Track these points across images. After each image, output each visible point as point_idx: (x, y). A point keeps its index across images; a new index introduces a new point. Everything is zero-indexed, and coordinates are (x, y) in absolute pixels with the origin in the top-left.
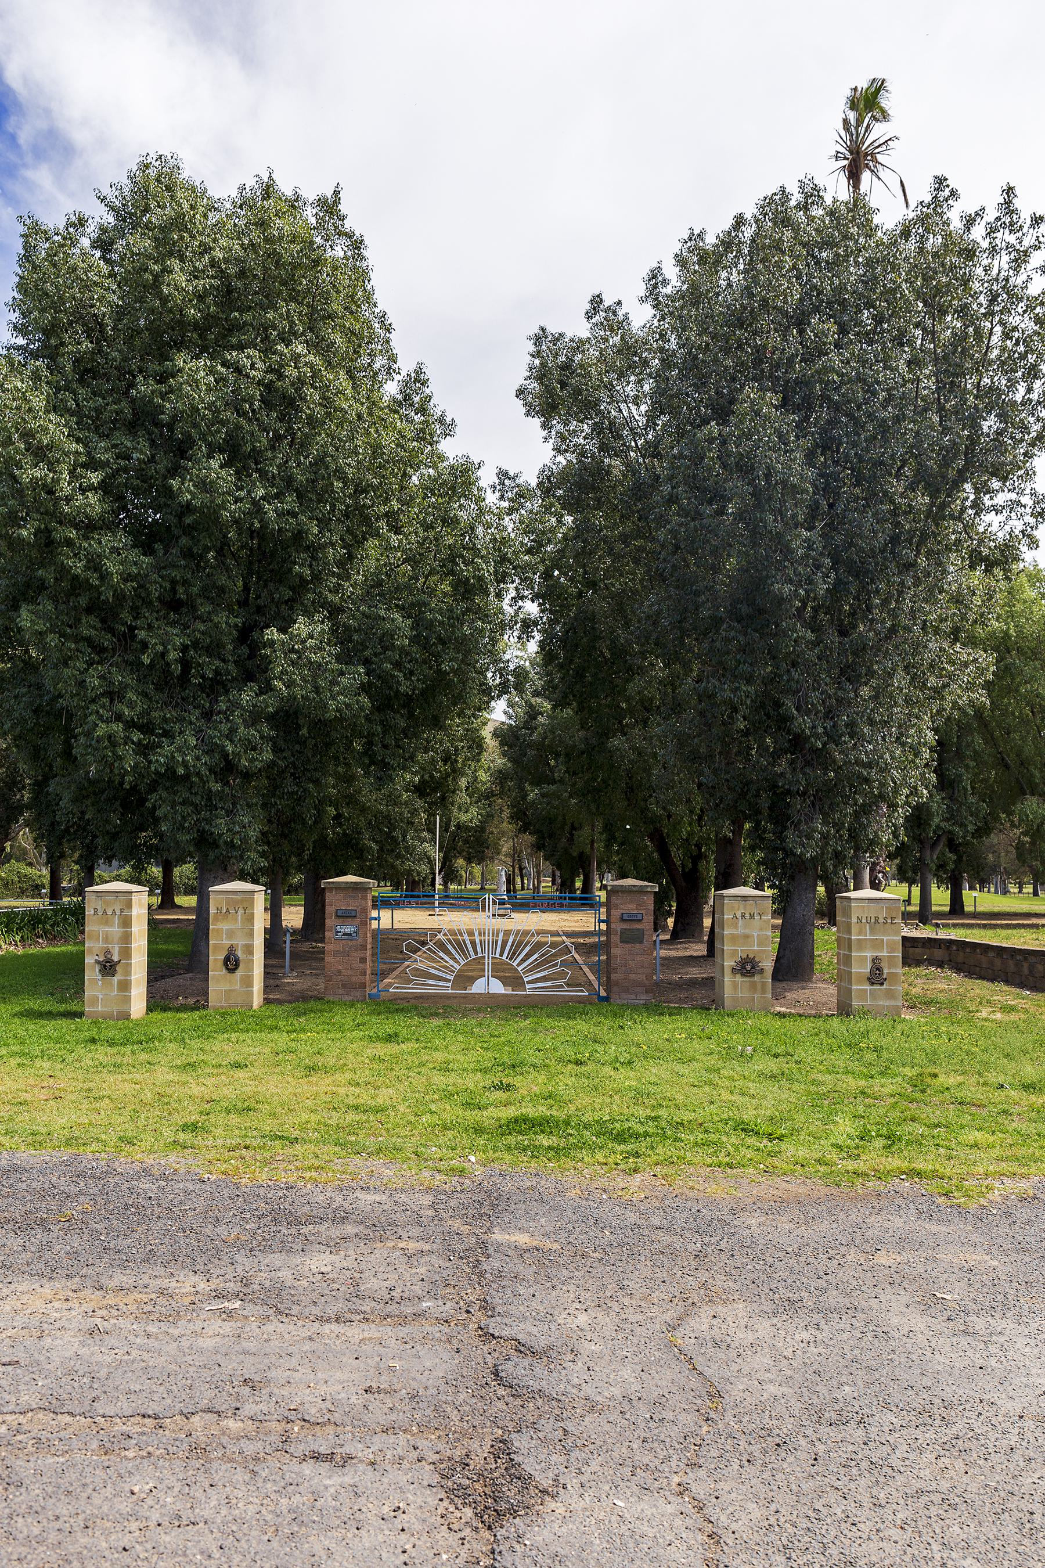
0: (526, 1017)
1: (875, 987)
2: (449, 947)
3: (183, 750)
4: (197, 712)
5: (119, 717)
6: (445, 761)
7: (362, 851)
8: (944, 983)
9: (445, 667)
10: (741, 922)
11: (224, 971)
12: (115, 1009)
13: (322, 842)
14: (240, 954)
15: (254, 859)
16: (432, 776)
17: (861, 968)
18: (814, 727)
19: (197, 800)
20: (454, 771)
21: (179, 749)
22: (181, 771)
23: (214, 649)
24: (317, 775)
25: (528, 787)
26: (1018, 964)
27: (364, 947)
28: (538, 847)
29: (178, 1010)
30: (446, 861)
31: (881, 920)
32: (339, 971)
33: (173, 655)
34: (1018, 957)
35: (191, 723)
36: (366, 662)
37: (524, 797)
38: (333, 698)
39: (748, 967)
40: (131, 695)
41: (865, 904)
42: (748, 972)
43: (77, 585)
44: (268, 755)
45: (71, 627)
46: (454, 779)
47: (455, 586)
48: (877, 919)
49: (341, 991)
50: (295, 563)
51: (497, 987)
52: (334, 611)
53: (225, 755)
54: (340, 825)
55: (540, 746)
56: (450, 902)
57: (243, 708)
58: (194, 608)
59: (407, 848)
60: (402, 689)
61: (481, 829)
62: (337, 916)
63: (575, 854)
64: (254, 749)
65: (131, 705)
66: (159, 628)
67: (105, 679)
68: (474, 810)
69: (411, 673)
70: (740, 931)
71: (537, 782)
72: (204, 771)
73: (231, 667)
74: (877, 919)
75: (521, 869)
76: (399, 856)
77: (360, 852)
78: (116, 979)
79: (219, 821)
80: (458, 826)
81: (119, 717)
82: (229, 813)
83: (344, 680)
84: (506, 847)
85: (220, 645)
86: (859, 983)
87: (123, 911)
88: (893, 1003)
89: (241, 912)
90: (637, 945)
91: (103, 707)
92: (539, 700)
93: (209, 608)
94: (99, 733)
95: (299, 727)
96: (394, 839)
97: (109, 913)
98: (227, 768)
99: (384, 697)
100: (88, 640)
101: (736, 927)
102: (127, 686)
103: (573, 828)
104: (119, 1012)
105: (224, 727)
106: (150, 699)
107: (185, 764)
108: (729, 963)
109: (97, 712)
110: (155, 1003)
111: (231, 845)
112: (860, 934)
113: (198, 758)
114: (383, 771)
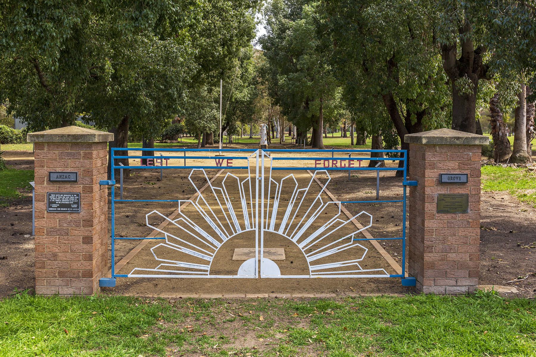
2: (208, 219)
6: (223, 45)
24: (58, 13)
25: (279, 77)
27: (89, 223)
28: (284, 113)
32: (55, 255)
37: (276, 84)
46: (230, 59)
49: (58, 281)
55: (287, 50)
61: (250, 102)
62: (50, 181)
63: (309, 116)
68: (246, 91)
71: (286, 72)
75: (272, 127)
84: (265, 115)
90: (459, 216)
92: (287, 20)
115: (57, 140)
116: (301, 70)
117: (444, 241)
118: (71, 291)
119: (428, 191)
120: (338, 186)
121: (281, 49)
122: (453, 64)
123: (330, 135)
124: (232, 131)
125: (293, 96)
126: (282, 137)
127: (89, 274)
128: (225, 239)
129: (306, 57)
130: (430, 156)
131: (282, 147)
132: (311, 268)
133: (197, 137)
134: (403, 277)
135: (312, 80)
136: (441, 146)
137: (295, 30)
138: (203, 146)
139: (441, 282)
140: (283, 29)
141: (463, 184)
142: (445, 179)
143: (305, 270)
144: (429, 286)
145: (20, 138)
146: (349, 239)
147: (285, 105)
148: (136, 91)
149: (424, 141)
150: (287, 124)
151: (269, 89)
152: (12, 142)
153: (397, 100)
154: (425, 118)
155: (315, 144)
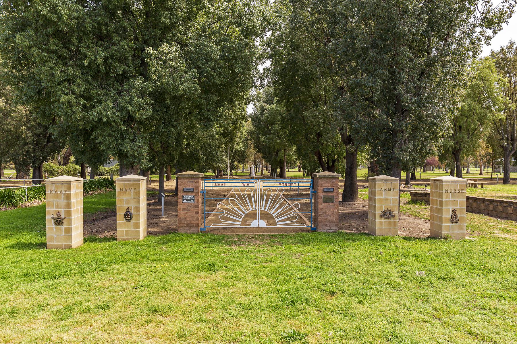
0: (281, 243)
1: (453, 224)
3: (107, 109)
4: (114, 91)
5: (73, 92)
6: (233, 124)
7: (198, 159)
8: (479, 219)
9: (237, 71)
10: (384, 193)
11: (125, 221)
12: (63, 243)
13: (181, 155)
14: (132, 211)
15: (146, 163)
16: (228, 130)
17: (447, 215)
18: (411, 99)
19: (115, 134)
20: (236, 128)
21: (104, 109)
22: (105, 120)
23: (123, 60)
26: (487, 206)
27: (197, 206)
29: (101, 241)
30: (232, 163)
31: (457, 191)
32: (185, 218)
33: (99, 61)
34: (486, 203)
35: (111, 96)
36: (199, 68)
37: (259, 140)
38: (181, 84)
39: (388, 214)
40: (79, 81)
41: (449, 183)
42: (388, 216)
43: (48, 22)
44: (150, 112)
45: (45, 45)
46: (236, 131)
47: (242, 31)
48: (455, 191)
49: (186, 228)
50: (162, 16)
51: (263, 224)
52: (183, 45)
53: (128, 112)
54: (189, 148)
55: (266, 121)
56: (233, 178)
57: (136, 88)
58: (111, 39)
59: (218, 158)
60: (216, 81)
63: (278, 160)
64: (143, 109)
65: (79, 86)
66: (92, 47)
67: (65, 73)
68: (241, 144)
69: (220, 74)
70: (384, 197)
71: (264, 134)
72: (118, 120)
73: (132, 69)
74: (455, 191)
76: (215, 161)
77: (198, 160)
78: (63, 227)
79: (126, 145)
80: (236, 151)
81: (73, 92)
82: (132, 141)
83: (187, 76)
85: (126, 59)
86: (446, 222)
87: (67, 191)
88: (461, 231)
89: (133, 190)
90: (331, 204)
91: (65, 87)
92: (265, 104)
93: (119, 38)
94: (62, 100)
95: (165, 99)
96: (213, 154)
97: (59, 192)
98: (129, 119)
99: (208, 88)
100: (55, 52)
101: (382, 195)
102: (77, 76)
103: (278, 151)
104: (65, 245)
105: (127, 98)
106: (90, 84)
107: (107, 116)
108: (378, 212)
109: (62, 89)
110: (89, 238)
111: (133, 156)
112: (446, 198)
113: (114, 113)
114: (207, 122)
115: (186, 176)
116: (274, 134)
117: (325, 213)
118: (191, 231)
119: (319, 194)
120: (292, 198)
121: (262, 121)
122: (345, 137)
123: (291, 170)
124: (233, 168)
125: (269, 148)
126: (262, 171)
127: (197, 225)
128: (241, 220)
129: (276, 126)
130: (320, 182)
131: (262, 178)
132: (277, 224)
133: (214, 172)
134: (311, 227)
135: (280, 139)
136: (324, 178)
137: (270, 110)
138: (217, 177)
139: (325, 228)
140: (263, 109)
141: (332, 192)
142: (325, 190)
143: (276, 225)
144: (320, 230)
145: (109, 173)
146: (291, 213)
147: (264, 153)
148: (197, 152)
149: (318, 176)
150: (265, 163)
151: (254, 143)
152: (62, 174)
153: (322, 154)
154: (336, 163)
155: (282, 176)
